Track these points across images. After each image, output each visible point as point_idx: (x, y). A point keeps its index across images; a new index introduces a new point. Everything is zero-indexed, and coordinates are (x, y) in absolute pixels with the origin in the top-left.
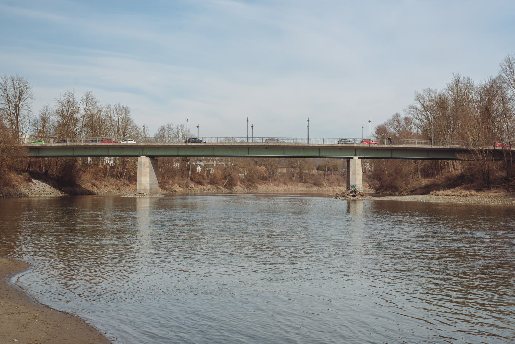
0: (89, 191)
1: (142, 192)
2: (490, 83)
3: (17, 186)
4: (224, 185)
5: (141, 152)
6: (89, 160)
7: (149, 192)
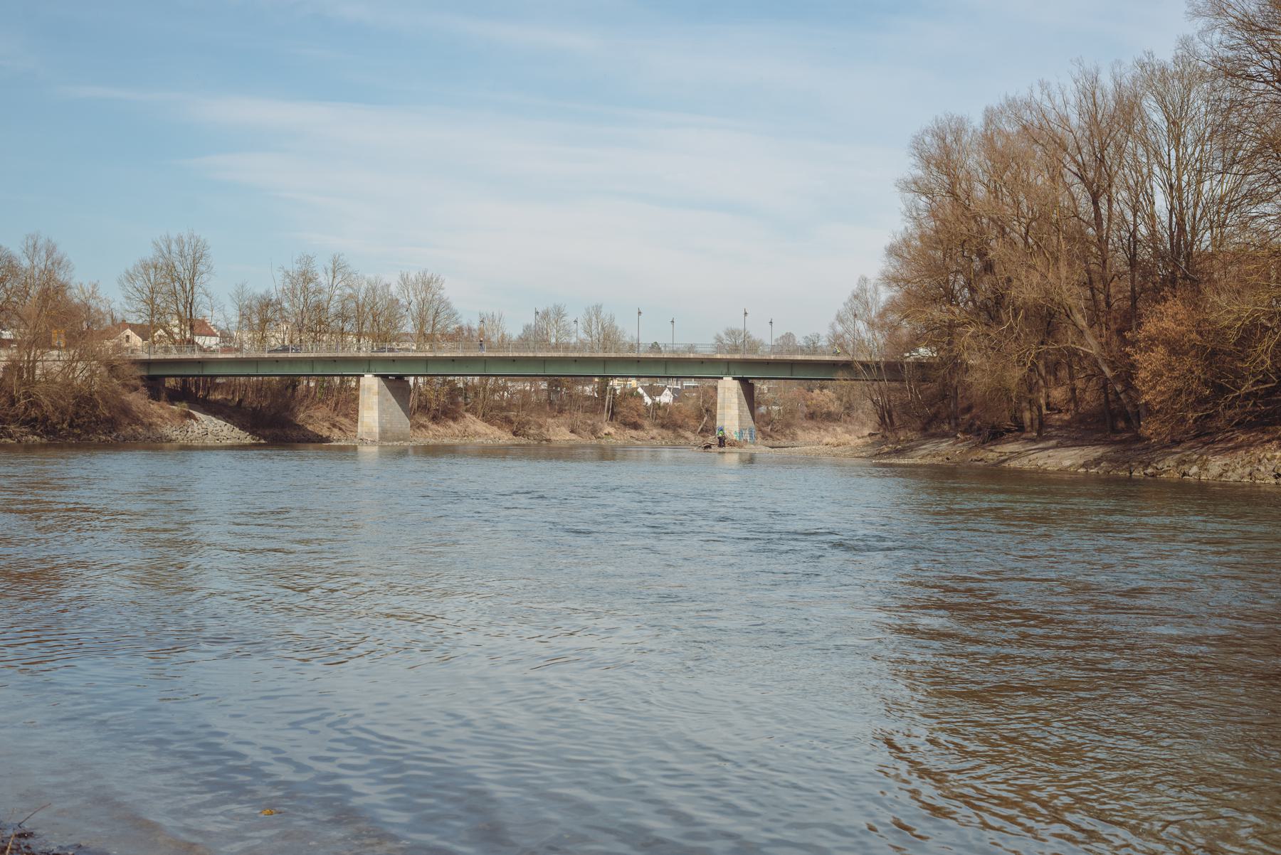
0: (318, 436)
1: (364, 437)
2: (927, 161)
3: (157, 425)
4: (699, 430)
5: (725, 371)
6: (337, 380)
7: (377, 437)
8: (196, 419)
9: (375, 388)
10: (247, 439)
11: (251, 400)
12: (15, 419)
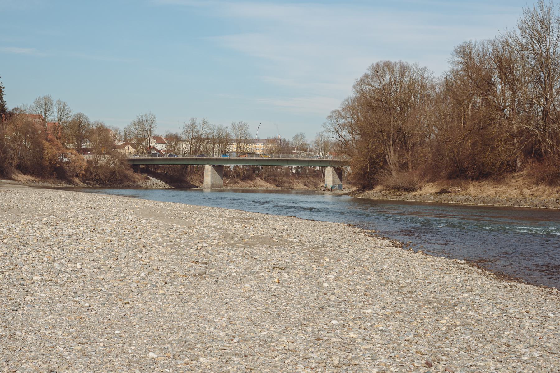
7: (210, 186)
8: (150, 180)
9: (210, 169)
10: (167, 186)
11: (171, 173)
12: (92, 179)
